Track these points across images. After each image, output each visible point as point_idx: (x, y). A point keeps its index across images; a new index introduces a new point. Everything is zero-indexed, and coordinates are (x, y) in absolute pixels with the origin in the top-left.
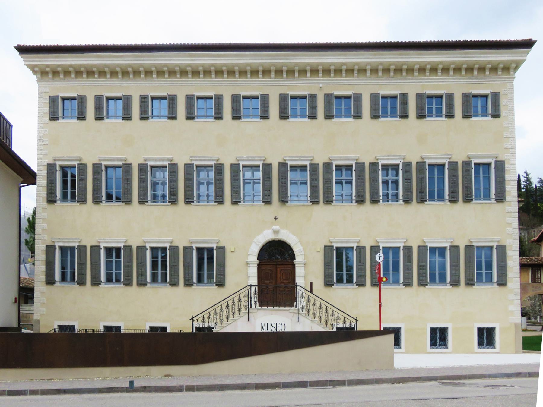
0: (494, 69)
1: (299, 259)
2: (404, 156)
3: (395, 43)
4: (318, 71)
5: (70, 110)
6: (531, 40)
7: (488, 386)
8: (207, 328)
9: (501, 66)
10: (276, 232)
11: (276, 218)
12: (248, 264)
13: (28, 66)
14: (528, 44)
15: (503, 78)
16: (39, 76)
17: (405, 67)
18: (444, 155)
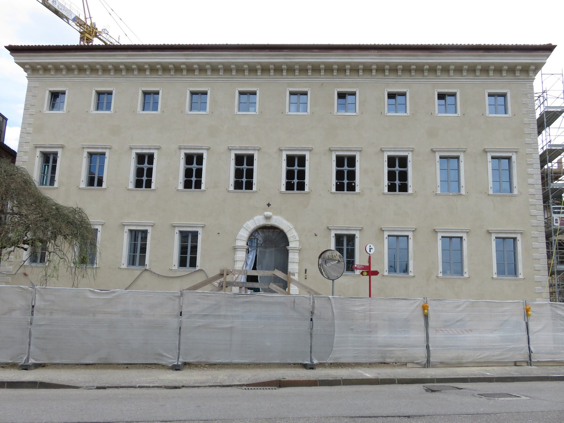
0: (512, 69)
1: (293, 245)
2: (412, 148)
3: (386, 45)
4: (377, 70)
6: (550, 44)
9: (519, 67)
10: (268, 218)
12: (235, 249)
14: (549, 48)
15: (429, 79)
17: (413, 67)
18: (458, 148)
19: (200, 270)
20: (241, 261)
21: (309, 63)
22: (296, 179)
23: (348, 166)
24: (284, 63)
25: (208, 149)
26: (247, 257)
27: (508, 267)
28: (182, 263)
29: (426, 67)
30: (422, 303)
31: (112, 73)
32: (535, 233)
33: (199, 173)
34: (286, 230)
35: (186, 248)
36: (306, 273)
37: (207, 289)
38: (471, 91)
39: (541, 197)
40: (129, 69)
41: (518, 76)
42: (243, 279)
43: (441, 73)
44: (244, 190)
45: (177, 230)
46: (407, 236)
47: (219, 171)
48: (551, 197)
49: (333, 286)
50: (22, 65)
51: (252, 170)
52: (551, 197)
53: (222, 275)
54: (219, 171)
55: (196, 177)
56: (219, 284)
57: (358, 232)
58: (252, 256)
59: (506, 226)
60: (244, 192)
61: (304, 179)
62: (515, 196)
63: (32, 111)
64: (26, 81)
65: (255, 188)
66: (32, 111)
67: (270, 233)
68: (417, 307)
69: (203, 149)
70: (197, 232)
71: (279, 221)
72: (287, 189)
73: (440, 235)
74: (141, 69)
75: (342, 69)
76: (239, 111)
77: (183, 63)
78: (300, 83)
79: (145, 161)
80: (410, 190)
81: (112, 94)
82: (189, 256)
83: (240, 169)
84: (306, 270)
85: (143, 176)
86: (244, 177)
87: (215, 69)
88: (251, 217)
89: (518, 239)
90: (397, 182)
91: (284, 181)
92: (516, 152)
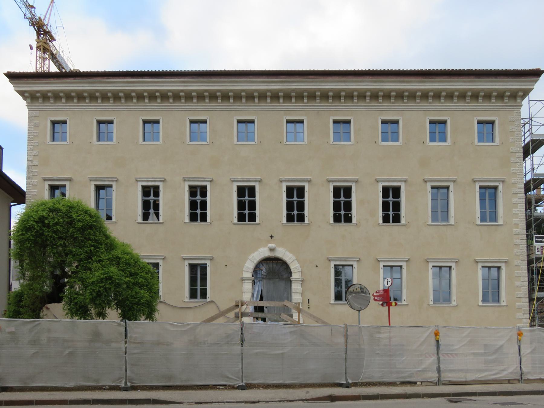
0: (501, 96)
2: (406, 179)
5: (60, 133)
6: (539, 69)
7: (499, 404)
8: (41, 308)
9: (508, 94)
10: (272, 250)
11: (272, 237)
12: (243, 280)
13: (18, 92)
14: (536, 74)
16: (29, 101)
18: (448, 178)
19: (211, 302)
20: (247, 293)
21: (306, 90)
22: (295, 212)
23: (345, 197)
24: (281, 90)
25: (211, 181)
26: (253, 288)
27: (492, 293)
28: (193, 295)
29: (419, 94)
30: (434, 331)
31: (170, 101)
32: (517, 262)
33: (204, 205)
34: (289, 262)
35: (196, 278)
36: (309, 303)
37: (221, 321)
38: (463, 119)
39: (524, 226)
40: (128, 96)
41: (506, 103)
42: (251, 309)
43: (433, 100)
44: (199, 221)
45: (187, 263)
46: (401, 266)
47: (222, 203)
48: (533, 227)
49: (359, 316)
50: (22, 93)
51: (254, 202)
52: (533, 227)
53: (237, 306)
54: (222, 203)
55: (201, 210)
56: (235, 313)
57: (356, 262)
58: (258, 287)
59: (492, 256)
60: (247, 224)
61: (303, 210)
62: (501, 225)
63: (36, 141)
64: (26, 111)
65: (257, 220)
66: (36, 141)
67: (271, 265)
68: (430, 333)
69: (206, 181)
70: (206, 264)
71: (282, 253)
72: (288, 221)
73: (431, 265)
74: (140, 96)
75: (337, 96)
76: (190, 141)
77: (182, 91)
78: (296, 111)
79: (150, 192)
80: (403, 221)
81: (66, 123)
82: (199, 287)
83: (242, 200)
84: (309, 300)
85: (197, 209)
86: (247, 210)
87: (213, 96)
88: (255, 249)
89: (502, 267)
90: (391, 213)
91: (284, 212)
92: (503, 182)
